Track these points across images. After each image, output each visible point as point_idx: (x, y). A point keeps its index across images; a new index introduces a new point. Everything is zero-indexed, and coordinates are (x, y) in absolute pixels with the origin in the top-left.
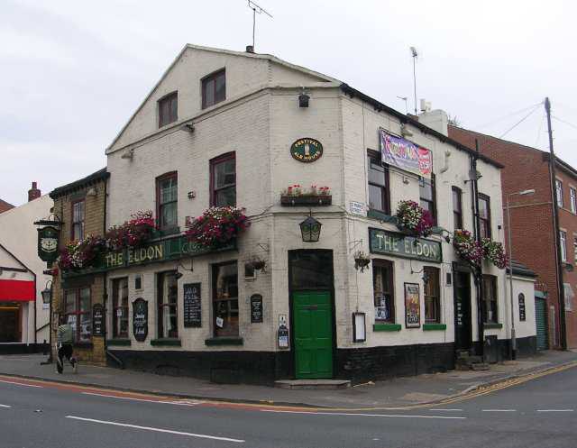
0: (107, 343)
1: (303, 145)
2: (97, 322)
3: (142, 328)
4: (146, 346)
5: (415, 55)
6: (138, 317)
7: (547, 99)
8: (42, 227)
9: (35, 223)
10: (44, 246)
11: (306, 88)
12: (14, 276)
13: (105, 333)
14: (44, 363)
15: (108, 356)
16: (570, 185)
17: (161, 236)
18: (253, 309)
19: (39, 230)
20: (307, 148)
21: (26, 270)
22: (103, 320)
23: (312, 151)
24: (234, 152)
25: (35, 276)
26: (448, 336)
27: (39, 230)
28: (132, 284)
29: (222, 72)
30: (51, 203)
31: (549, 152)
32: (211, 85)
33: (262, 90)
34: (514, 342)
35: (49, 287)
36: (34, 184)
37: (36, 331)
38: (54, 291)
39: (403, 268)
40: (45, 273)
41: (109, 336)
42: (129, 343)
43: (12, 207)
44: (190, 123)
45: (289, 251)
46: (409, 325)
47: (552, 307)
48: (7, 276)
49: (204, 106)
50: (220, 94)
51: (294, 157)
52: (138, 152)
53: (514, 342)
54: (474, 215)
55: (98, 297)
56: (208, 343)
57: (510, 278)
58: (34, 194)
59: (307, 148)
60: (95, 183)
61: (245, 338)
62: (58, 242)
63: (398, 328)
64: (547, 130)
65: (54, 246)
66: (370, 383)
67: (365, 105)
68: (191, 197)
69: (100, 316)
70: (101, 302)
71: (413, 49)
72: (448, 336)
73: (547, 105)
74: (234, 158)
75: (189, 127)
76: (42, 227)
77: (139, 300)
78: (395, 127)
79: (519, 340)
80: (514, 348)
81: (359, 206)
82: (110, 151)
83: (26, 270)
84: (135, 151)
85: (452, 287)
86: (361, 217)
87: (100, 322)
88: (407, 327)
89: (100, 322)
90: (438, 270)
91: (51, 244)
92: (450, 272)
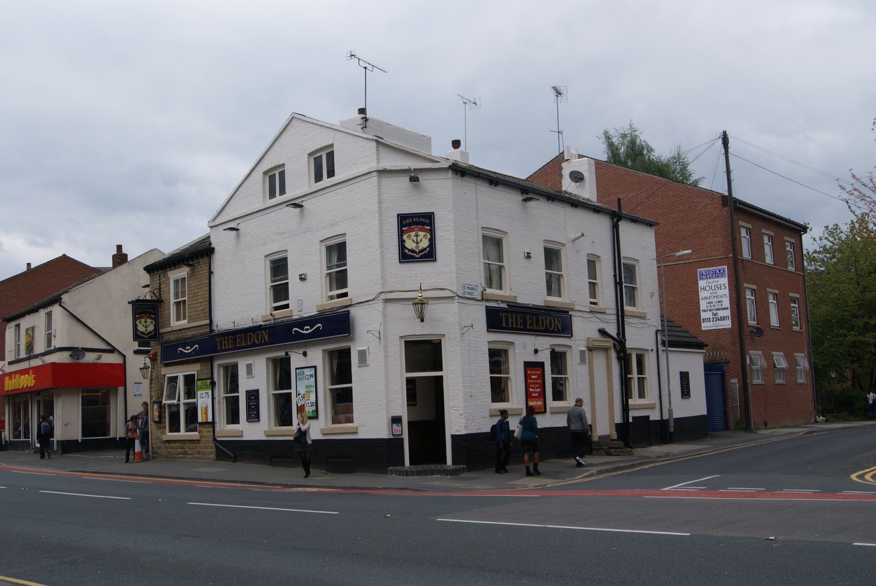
5: (558, 93)
10: (141, 328)
12: (99, 358)
16: (764, 231)
21: (112, 350)
25: (124, 357)
30: (146, 278)
31: (726, 194)
33: (370, 172)
34: (672, 424)
36: (119, 248)
40: (137, 352)
47: (734, 381)
53: (672, 424)
54: (616, 283)
58: (120, 258)
64: (725, 170)
65: (151, 328)
67: (477, 183)
68: (302, 278)
79: (677, 420)
80: (672, 430)
82: (214, 224)
83: (112, 350)
91: (147, 326)
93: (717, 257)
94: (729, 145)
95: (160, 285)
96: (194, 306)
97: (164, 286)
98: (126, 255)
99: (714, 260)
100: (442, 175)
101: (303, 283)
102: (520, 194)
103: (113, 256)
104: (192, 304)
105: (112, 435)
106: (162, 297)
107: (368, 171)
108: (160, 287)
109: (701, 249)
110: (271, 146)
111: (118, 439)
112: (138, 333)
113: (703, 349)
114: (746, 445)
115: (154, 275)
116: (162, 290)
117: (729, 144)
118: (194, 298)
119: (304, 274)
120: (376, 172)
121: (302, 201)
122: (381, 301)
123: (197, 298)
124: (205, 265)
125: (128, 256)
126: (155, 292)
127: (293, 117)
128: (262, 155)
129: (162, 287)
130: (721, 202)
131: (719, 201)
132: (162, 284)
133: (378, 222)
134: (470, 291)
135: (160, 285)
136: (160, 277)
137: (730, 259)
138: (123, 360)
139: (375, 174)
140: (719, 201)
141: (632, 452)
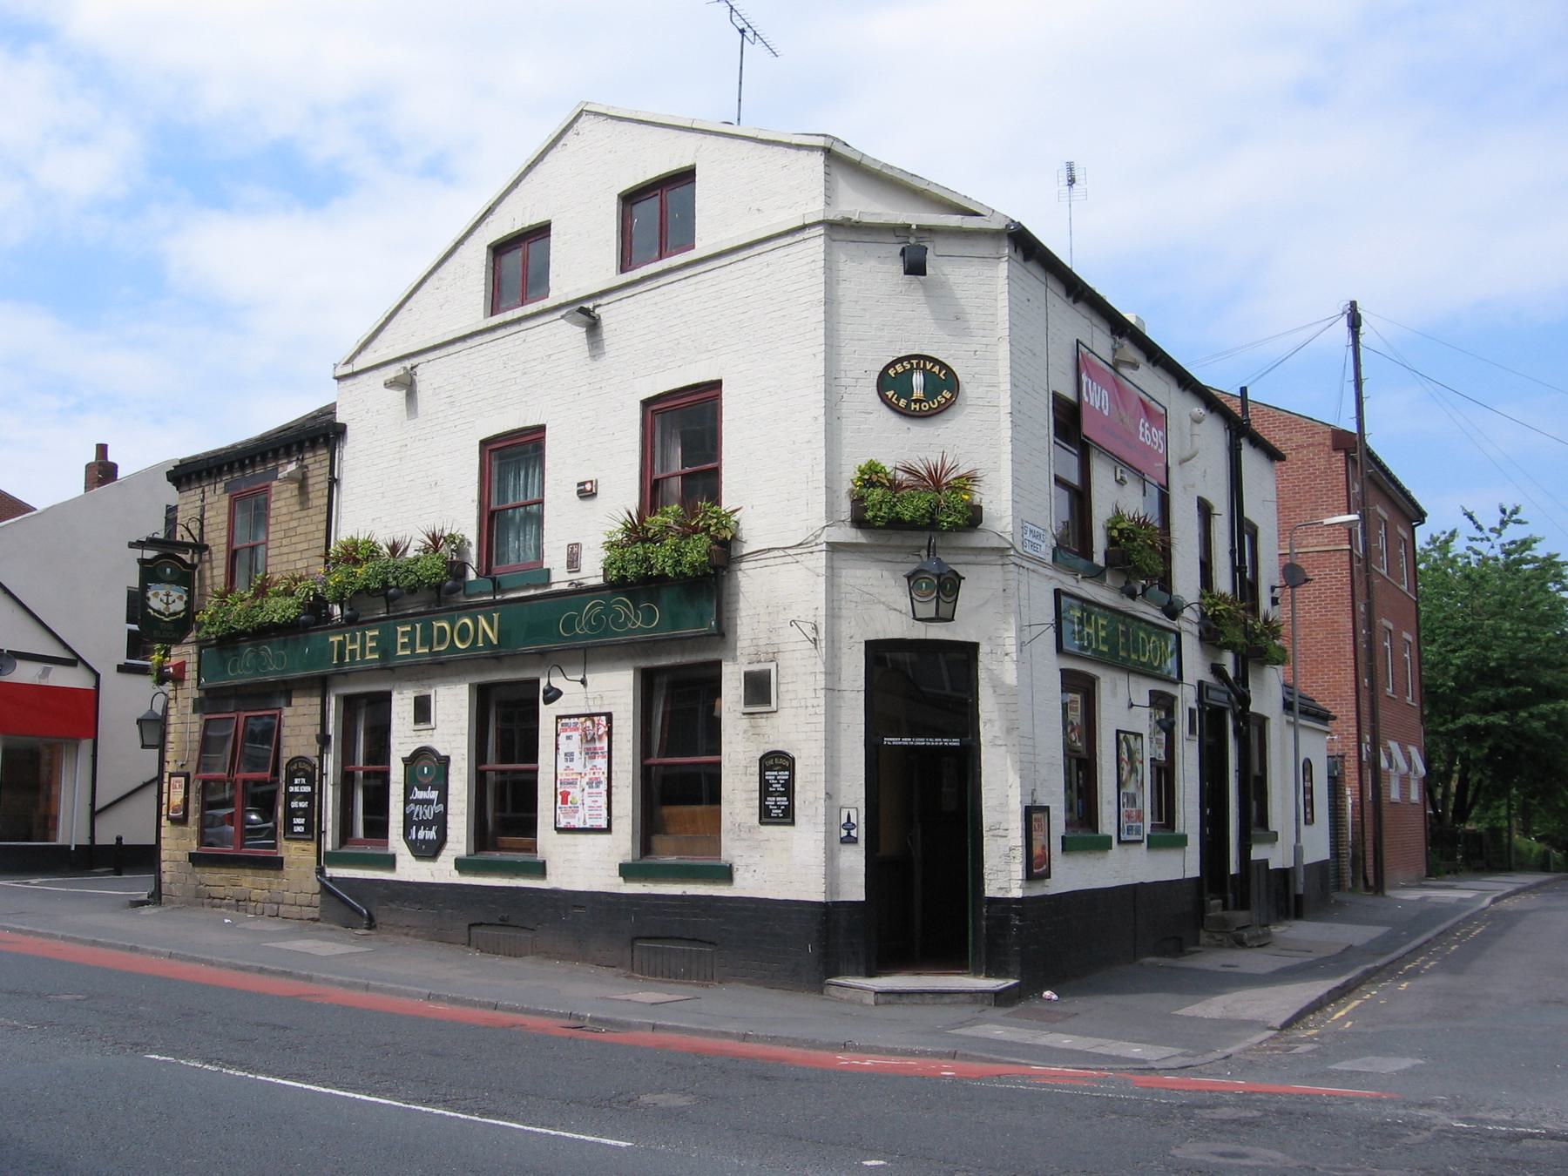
0: (325, 860)
1: (908, 374)
2: (294, 805)
3: (427, 824)
4: (442, 871)
6: (420, 795)
7: (1353, 304)
8: (150, 554)
9: (131, 545)
11: (920, 228)
12: (46, 673)
13: (321, 833)
14: (142, 903)
15: (325, 891)
17: (494, 593)
18: (765, 789)
19: (142, 562)
20: (918, 379)
22: (314, 799)
23: (932, 388)
24: (717, 384)
25: (97, 676)
26: (1185, 864)
27: (142, 562)
28: (402, 706)
29: (686, 176)
31: (1354, 429)
32: (513, 260)
35: (158, 710)
36: (102, 449)
37: (94, 814)
38: (172, 719)
39: (1114, 694)
40: (122, 669)
41: (329, 844)
42: (390, 862)
43: (31, 509)
44: (589, 305)
45: (868, 644)
46: (1124, 837)
48: (26, 674)
49: (625, 265)
50: (534, 282)
51: (885, 400)
52: (429, 375)
55: (302, 741)
56: (627, 871)
57: (1294, 724)
59: (918, 379)
60: (301, 450)
61: (738, 863)
62: (190, 593)
63: (1104, 844)
65: (179, 606)
66: (1047, 994)
69: (308, 789)
70: (311, 751)
71: (1070, 169)
72: (1185, 864)
73: (1355, 322)
74: (718, 397)
75: (586, 315)
76: (150, 554)
77: (422, 754)
78: (1101, 342)
81: (1037, 536)
82: (348, 370)
83: (74, 660)
84: (418, 370)
85: (1197, 744)
86: (1041, 562)
87: (304, 805)
88: (1120, 842)
89: (304, 805)
90: (1174, 698)
92: (1195, 706)
93: (1317, 549)
94: (1362, 330)
95: (203, 509)
96: (285, 558)
97: (212, 513)
98: (114, 467)
99: (1310, 554)
100: (986, 248)
101: (588, 504)
102: (1109, 333)
103: (87, 466)
104: (280, 554)
105: (61, 840)
106: (205, 539)
107: (800, 223)
108: (202, 516)
109: (1284, 530)
110: (516, 183)
111: (73, 848)
112: (151, 611)
113: (1327, 725)
114: (693, 859)
115: (190, 490)
116: (205, 522)
117: (1361, 328)
118: (284, 542)
119: (591, 482)
120: (820, 230)
121: (595, 307)
122: (824, 547)
123: (294, 540)
124: (317, 465)
125: (119, 469)
126: (190, 527)
127: (582, 110)
128: (490, 204)
129: (206, 515)
130: (1329, 442)
131: (1325, 439)
132: (208, 511)
133: (823, 348)
134: (1034, 540)
135: (203, 509)
136: (203, 492)
137: (1344, 552)
138: (94, 685)
139: (820, 230)
140: (1325, 439)
141: (1269, 934)
